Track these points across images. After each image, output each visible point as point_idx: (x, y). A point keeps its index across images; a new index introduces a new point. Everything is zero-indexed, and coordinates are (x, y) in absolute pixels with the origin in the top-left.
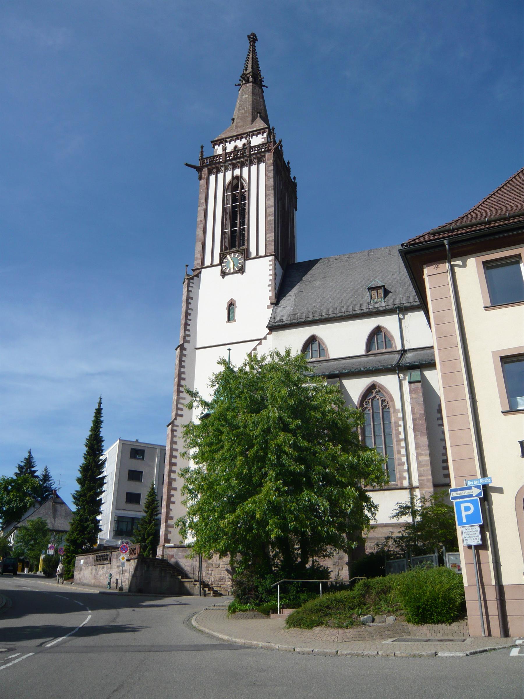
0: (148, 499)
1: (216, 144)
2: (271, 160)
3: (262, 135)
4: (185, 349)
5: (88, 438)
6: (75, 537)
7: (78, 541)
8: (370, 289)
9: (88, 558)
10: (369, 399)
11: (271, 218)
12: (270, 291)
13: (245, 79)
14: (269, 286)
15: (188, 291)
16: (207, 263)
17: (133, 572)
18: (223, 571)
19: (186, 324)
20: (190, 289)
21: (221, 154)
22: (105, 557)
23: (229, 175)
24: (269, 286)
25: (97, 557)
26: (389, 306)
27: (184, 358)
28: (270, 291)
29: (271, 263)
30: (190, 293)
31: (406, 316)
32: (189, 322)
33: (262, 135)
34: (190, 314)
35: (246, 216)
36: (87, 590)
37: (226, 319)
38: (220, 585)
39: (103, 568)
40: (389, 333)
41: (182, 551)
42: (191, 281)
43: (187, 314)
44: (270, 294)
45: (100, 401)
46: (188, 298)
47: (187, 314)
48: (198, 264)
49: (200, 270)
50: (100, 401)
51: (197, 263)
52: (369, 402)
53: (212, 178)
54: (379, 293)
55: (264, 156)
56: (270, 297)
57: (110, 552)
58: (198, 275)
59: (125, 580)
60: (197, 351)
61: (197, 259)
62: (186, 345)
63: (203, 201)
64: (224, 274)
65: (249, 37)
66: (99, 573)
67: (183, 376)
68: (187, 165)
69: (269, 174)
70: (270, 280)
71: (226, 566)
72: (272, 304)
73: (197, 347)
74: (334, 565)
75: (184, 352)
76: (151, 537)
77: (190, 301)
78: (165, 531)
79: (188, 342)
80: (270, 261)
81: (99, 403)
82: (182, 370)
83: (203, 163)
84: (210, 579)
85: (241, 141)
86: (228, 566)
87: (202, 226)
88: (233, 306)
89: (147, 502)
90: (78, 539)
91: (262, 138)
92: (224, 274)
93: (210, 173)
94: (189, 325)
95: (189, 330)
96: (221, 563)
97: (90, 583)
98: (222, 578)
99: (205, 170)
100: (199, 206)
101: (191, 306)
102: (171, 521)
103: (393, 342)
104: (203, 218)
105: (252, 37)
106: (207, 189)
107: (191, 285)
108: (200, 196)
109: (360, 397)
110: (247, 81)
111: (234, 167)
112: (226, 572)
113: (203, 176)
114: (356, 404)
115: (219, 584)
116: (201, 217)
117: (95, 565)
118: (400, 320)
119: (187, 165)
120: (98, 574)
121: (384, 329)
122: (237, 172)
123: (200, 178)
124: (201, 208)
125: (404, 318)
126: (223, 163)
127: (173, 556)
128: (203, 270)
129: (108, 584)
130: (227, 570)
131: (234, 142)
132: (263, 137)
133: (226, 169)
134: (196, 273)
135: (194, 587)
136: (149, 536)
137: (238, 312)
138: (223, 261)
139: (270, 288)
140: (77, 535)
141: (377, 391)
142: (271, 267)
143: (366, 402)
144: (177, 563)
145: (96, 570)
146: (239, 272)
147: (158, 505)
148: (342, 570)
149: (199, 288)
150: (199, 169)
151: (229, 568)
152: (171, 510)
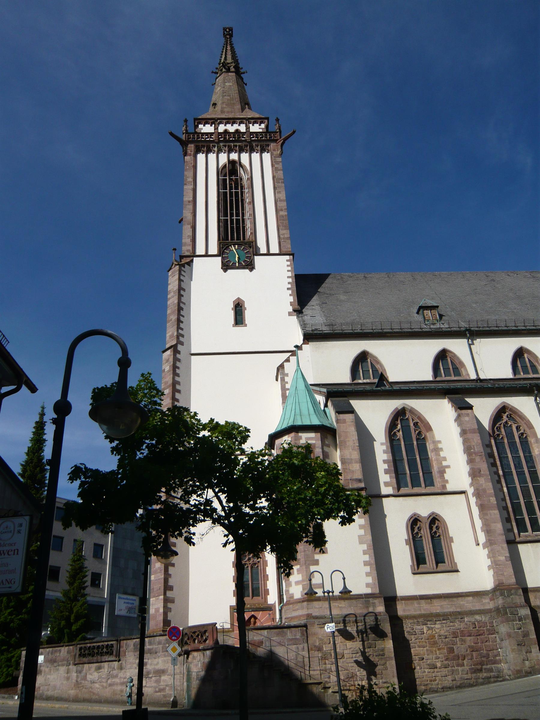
0: (71, 565)
1: (200, 123)
2: (278, 151)
3: (260, 125)
4: (179, 352)
5: (24, 463)
6: (6, 618)
7: (12, 625)
8: (422, 308)
9: (56, 651)
10: (500, 424)
11: (284, 213)
12: (290, 295)
13: (225, 67)
14: (288, 289)
15: (180, 280)
16: (200, 249)
17: (203, 673)
18: (350, 665)
19: (179, 321)
20: (182, 278)
21: (213, 133)
22: (105, 650)
23: (223, 158)
24: (288, 289)
25: (81, 649)
26: (455, 328)
27: (178, 364)
28: (290, 295)
29: (289, 263)
30: (182, 282)
31: (474, 341)
32: (182, 318)
33: (260, 125)
34: (182, 309)
35: (247, 207)
36: (102, 708)
37: (232, 321)
38: (348, 688)
39: (99, 668)
40: (458, 358)
41: (278, 634)
42: (183, 268)
43: (180, 309)
44: (291, 299)
45: (43, 411)
46: (180, 289)
47: (180, 309)
48: (188, 251)
49: (192, 258)
50: (43, 411)
51: (186, 250)
52: (500, 427)
53: (201, 157)
54: (433, 314)
55: (268, 145)
56: (291, 302)
57: (117, 640)
58: (190, 263)
59: (162, 687)
60: (193, 357)
61: (186, 244)
62: (180, 347)
63: (190, 179)
64: (226, 267)
65: (225, 29)
66: (89, 677)
67: (178, 387)
68: (171, 134)
69: (276, 166)
70: (289, 283)
71: (354, 655)
72: (294, 311)
73: (193, 352)
74: (518, 645)
75: (178, 356)
76: (82, 621)
77: (182, 292)
78: (164, 607)
79: (182, 344)
80: (287, 261)
81: (40, 414)
82: (177, 379)
83: (188, 138)
84: (329, 677)
85: (232, 125)
86: (358, 655)
87: (191, 207)
88: (241, 307)
89: (72, 570)
90: (12, 621)
91: (260, 128)
92: (226, 267)
93: (198, 150)
94: (182, 322)
95: (182, 329)
96: (345, 652)
97: (65, 696)
98: (350, 676)
99: (191, 147)
100: (186, 184)
101: (183, 299)
102: (171, 592)
103: (463, 370)
104: (191, 199)
105: (227, 30)
106: (195, 167)
107: (183, 273)
108: (186, 173)
109: (490, 419)
110: (228, 71)
111: (230, 151)
112: (355, 665)
113: (189, 152)
114: (487, 429)
115: (346, 686)
116: (188, 197)
117: (75, 665)
118: (470, 345)
119: (171, 134)
120: (85, 678)
121: (450, 354)
122: (234, 156)
123: (185, 154)
124: (188, 188)
125: (473, 344)
126: (216, 143)
127: (261, 643)
128: (195, 259)
129: (128, 697)
130: (357, 662)
131: (223, 125)
132: (260, 127)
133: (219, 151)
134: (188, 260)
135: (325, 692)
136: (77, 618)
137: (248, 315)
138: (223, 252)
139: (290, 292)
140: (10, 614)
141: (507, 415)
142: (290, 268)
143: (497, 428)
144: (271, 655)
145: (79, 672)
146: (247, 268)
147: (87, 574)
148: (531, 652)
149: (192, 280)
150: (184, 144)
151: (360, 659)
152: (170, 575)
